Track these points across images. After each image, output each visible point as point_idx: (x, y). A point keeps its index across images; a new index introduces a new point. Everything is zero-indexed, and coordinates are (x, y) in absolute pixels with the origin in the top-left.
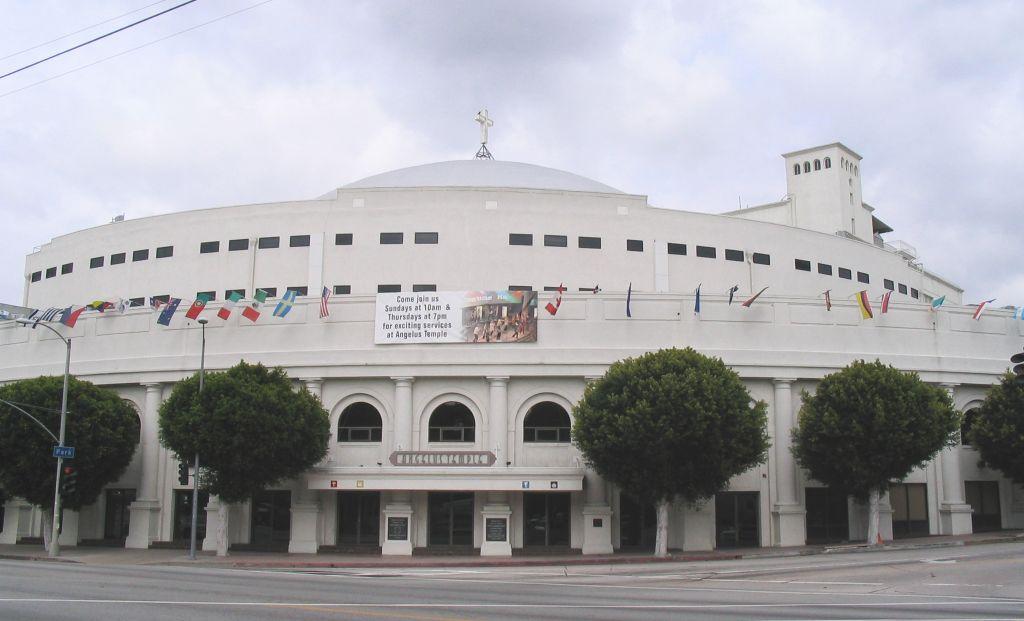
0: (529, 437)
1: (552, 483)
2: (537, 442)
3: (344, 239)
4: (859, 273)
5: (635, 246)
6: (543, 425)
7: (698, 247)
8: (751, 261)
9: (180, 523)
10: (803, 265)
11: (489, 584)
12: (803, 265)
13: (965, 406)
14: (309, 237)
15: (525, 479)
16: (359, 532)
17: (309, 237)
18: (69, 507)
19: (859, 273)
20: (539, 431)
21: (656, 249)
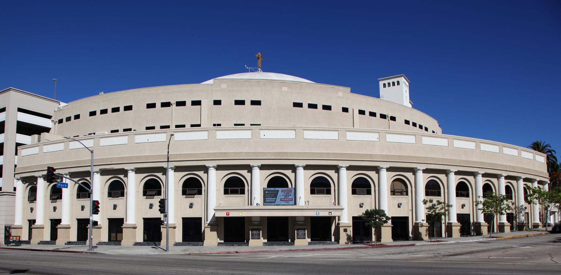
0: (312, 192)
1: (329, 213)
2: (230, 194)
3: (217, 103)
4: (413, 122)
5: (345, 110)
6: (199, 188)
7: (343, 108)
8: (389, 119)
9: (10, 235)
10: (407, 122)
11: (300, 253)
12: (407, 122)
13: (460, 179)
14: (201, 101)
15: (330, 211)
16: (491, 232)
17: (201, 101)
18: (461, 227)
19: (413, 122)
20: (231, 190)
21: (337, 109)
